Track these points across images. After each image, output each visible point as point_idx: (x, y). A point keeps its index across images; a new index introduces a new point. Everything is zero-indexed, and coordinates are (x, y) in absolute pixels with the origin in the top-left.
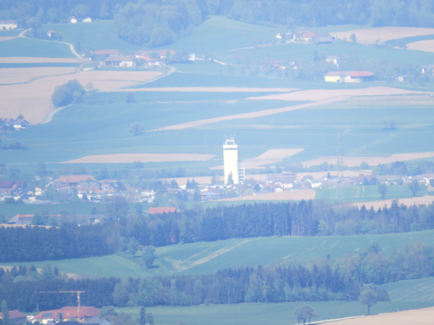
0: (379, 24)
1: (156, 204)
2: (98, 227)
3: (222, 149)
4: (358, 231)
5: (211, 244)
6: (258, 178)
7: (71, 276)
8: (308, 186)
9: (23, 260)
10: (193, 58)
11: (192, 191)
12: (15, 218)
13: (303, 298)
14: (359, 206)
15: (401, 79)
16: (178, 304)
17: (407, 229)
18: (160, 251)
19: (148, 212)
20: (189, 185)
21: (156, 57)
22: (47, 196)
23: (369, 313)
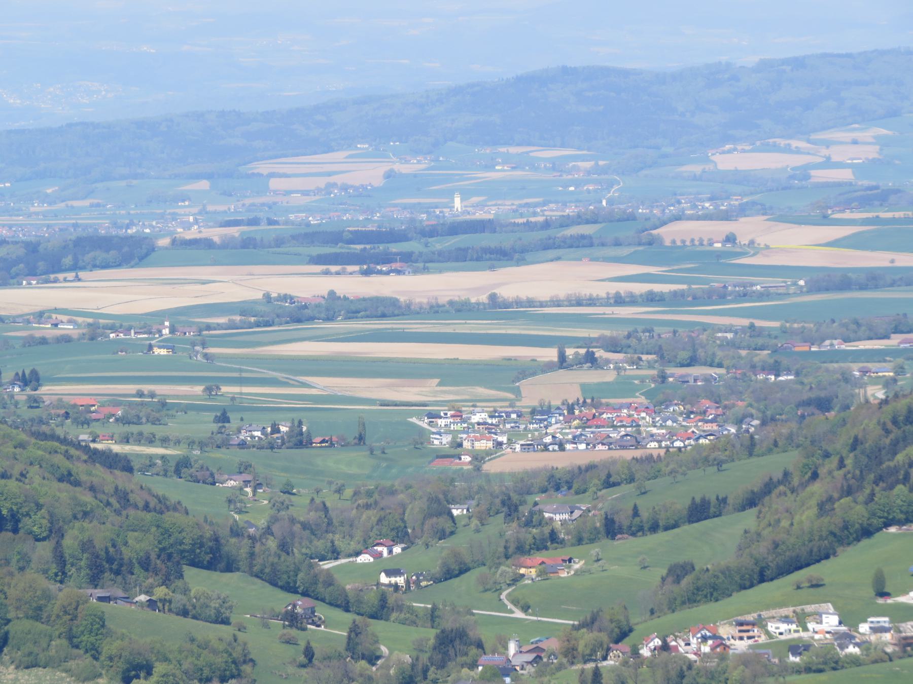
0: (518, 145)
1: (428, 220)
2: (405, 230)
3: (454, 197)
4: (512, 232)
5: (451, 237)
6: (469, 209)
7: (394, 250)
8: (490, 213)
9: (374, 243)
10: (441, 159)
11: (441, 214)
12: (370, 226)
13: (490, 259)
14: (513, 221)
15: (527, 168)
16: (439, 261)
17: (532, 231)
18: (430, 240)
19: (425, 223)
20: (440, 212)
21: (425, 158)
22: (382, 216)
23: (518, 266)
